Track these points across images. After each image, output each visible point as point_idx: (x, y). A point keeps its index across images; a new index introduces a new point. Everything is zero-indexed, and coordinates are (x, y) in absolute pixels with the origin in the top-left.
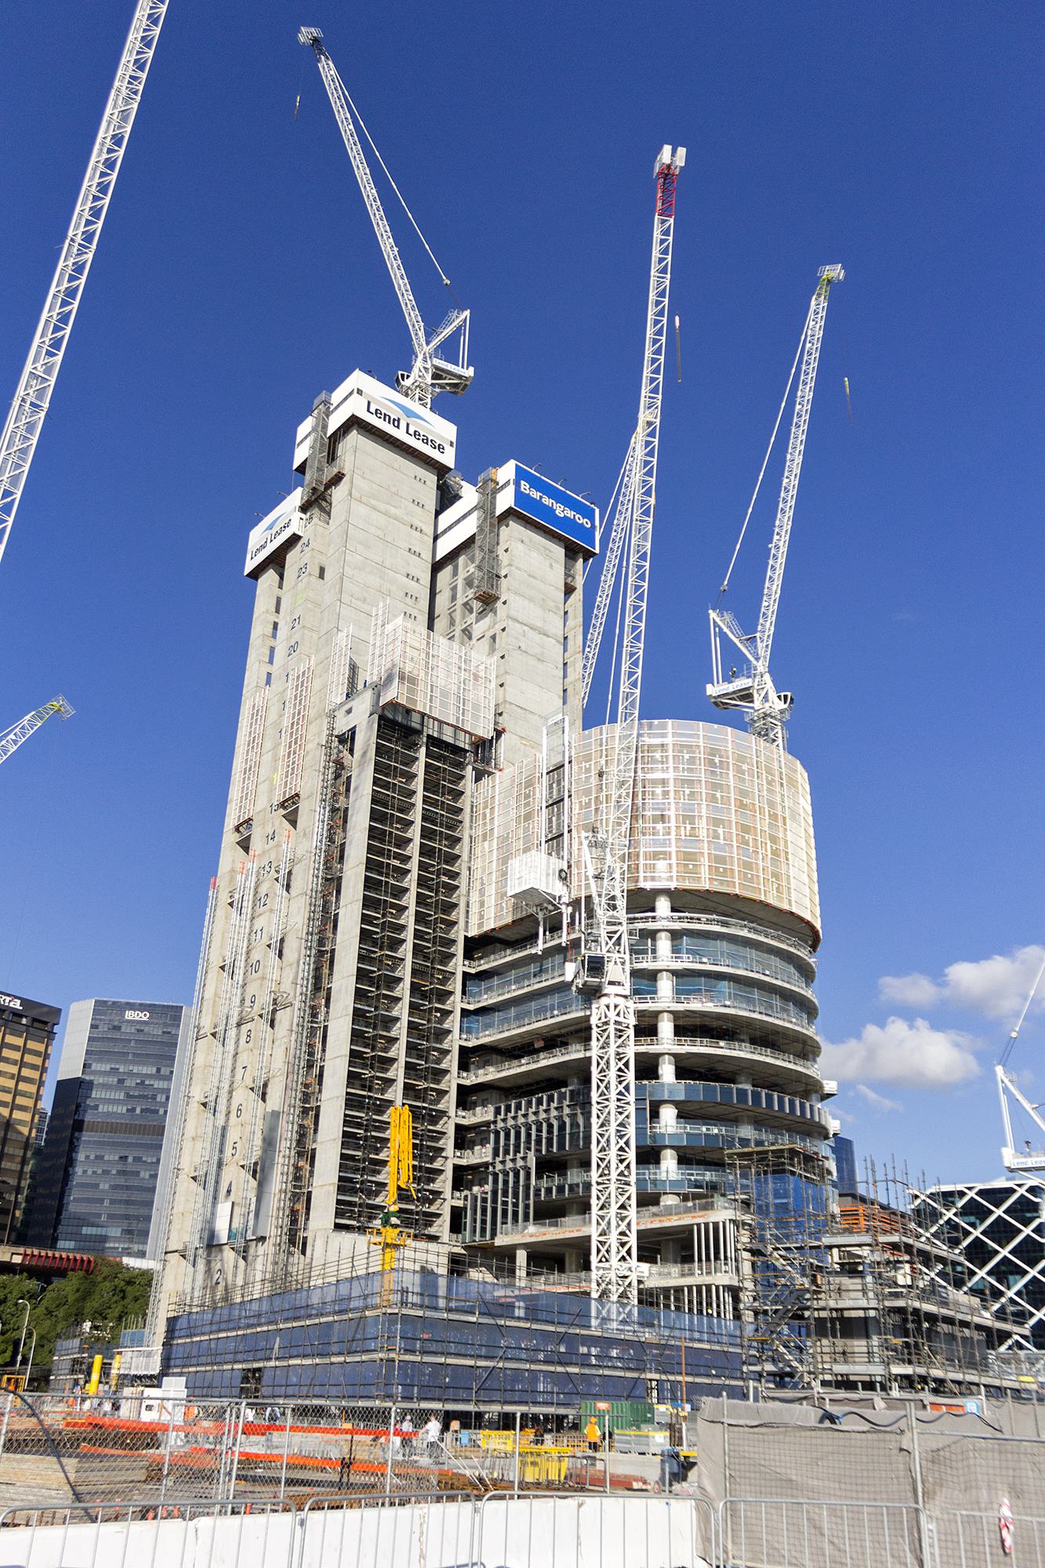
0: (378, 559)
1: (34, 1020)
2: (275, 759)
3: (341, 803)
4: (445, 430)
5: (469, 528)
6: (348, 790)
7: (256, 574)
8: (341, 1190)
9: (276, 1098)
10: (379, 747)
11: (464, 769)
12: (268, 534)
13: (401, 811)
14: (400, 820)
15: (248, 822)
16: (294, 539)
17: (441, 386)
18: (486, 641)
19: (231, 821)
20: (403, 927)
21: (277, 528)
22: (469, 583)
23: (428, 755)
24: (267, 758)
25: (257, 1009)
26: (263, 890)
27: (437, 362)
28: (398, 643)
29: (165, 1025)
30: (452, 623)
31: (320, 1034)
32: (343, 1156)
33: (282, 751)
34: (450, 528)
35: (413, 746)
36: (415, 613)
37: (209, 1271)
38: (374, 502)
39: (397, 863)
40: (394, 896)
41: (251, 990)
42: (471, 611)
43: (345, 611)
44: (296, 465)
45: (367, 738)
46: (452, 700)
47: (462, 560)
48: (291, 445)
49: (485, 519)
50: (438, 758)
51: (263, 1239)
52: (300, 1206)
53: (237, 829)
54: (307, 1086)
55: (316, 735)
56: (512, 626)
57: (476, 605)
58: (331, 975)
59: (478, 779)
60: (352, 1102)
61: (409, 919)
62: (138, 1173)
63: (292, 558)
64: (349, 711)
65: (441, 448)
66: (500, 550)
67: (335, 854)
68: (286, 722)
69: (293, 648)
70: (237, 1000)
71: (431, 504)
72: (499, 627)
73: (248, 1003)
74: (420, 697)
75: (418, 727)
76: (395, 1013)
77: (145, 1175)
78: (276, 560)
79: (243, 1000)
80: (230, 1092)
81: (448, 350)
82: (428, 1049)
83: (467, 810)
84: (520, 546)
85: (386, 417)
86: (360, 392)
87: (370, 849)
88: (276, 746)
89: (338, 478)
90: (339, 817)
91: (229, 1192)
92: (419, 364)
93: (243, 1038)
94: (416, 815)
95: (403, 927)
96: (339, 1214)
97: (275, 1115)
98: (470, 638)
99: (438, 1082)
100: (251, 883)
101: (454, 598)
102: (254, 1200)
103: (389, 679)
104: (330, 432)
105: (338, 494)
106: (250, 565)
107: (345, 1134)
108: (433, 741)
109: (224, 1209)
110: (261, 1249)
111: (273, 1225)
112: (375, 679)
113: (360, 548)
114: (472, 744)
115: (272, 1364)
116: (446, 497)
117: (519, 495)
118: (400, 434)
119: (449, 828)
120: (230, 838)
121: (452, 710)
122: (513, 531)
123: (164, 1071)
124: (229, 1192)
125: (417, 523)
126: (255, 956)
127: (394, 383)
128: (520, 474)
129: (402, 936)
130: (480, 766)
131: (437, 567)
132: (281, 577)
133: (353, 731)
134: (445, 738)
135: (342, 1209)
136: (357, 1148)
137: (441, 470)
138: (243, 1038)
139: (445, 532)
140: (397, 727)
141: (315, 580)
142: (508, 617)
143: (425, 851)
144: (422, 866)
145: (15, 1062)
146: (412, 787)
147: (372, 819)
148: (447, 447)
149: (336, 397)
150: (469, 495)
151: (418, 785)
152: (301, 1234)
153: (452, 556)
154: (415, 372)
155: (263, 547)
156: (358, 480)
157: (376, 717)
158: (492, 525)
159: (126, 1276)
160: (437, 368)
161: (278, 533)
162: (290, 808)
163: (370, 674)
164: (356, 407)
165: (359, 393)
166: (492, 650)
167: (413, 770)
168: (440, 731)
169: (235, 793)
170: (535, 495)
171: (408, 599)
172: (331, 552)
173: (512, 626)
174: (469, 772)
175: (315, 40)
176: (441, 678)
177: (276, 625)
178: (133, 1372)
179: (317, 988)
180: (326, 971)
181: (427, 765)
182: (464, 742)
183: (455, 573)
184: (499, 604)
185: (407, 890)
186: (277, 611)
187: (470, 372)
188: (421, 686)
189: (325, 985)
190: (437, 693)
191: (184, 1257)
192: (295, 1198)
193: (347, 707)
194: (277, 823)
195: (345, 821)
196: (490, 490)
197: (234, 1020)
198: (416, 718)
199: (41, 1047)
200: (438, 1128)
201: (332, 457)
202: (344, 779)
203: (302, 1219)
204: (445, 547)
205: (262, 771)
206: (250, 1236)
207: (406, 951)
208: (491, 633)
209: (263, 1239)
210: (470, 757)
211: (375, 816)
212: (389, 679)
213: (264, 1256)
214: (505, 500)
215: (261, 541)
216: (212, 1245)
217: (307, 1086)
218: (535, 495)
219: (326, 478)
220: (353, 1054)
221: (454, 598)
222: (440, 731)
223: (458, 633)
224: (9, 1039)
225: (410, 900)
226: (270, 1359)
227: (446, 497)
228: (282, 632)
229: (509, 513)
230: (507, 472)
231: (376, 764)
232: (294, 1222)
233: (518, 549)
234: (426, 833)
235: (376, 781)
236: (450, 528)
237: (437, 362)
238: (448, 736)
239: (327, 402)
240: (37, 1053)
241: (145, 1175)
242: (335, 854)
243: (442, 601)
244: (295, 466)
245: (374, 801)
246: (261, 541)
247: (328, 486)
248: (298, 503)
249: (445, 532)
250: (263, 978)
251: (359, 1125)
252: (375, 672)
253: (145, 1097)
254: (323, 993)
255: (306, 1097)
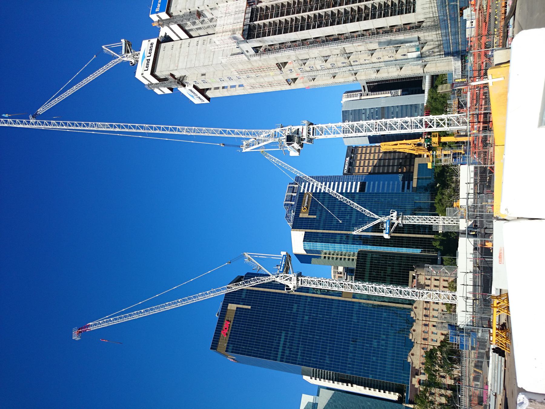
0: (195, 56)
1: (352, 153)
2: (266, 76)
3: (278, 46)
4: (146, 44)
5: (175, 27)
6: (272, 45)
7: (208, 99)
8: (402, 13)
9: (375, 46)
10: (257, 37)
11: (258, 8)
12: (195, 97)
13: (276, 25)
14: (280, 25)
15: (287, 81)
16: (195, 87)
17: (131, 50)
18: (213, 12)
19: (288, 87)
20: (315, 15)
21: (192, 94)
22: (194, 23)
23: (256, 20)
24: (266, 79)
25: (347, 61)
26: (308, 69)
27: (123, 52)
28: (223, 39)
29: (349, 115)
30: (209, 27)
31: (353, 34)
32: (391, 15)
33: (263, 74)
34: (177, 35)
35: (254, 26)
36: (209, 40)
37: (429, 56)
38: (177, 62)
39: (294, 23)
40: (305, 21)
41: (340, 65)
42: (204, 20)
43: (214, 62)
44: (170, 92)
45: (255, 42)
46: (236, 16)
47: (187, 28)
48: (165, 95)
49: (172, 22)
50: (256, 17)
51: (419, 38)
52: (408, 27)
53: (290, 84)
54: (370, 35)
55: (258, 61)
56: (206, 4)
57: (202, 19)
58: (332, 35)
59: (261, 2)
60: (373, 17)
61: (311, 14)
62: (397, 112)
63: (201, 87)
64: (247, 51)
65: (152, 44)
66: (181, 14)
67: (295, 45)
68: (253, 75)
69: (230, 79)
70: (344, 69)
71: (171, 43)
72: (208, 8)
73: (345, 65)
74: (238, 27)
75: (248, 26)
76: (343, 11)
77: (397, 110)
78: (202, 92)
79: (344, 67)
80: (373, 63)
81: (118, 50)
82: (351, 15)
83: (272, 3)
84: (178, 7)
85: (148, 64)
86: (142, 74)
87: (291, 31)
88: (262, 77)
89: (172, 75)
90: (282, 46)
91: (404, 55)
92: (125, 59)
93: (356, 63)
94: (277, 19)
95: (315, 15)
96: (410, 12)
97: (380, 43)
98: (213, 19)
99: (362, 9)
100: (307, 74)
101: (200, 28)
102: (406, 44)
103: (235, 38)
104: (158, 82)
105: (177, 75)
106: (206, 101)
107: (384, 16)
108: (251, 20)
109: (410, 55)
110: (422, 39)
111: (414, 35)
112: (235, 44)
113: (193, 62)
114: (249, 7)
115: (458, 4)
116: (168, 39)
117: (161, 11)
118: (152, 58)
119: (279, 8)
120: (293, 86)
121: (240, 15)
122: (174, 10)
123: (363, 111)
124: (404, 55)
125: (179, 46)
126: (330, 66)
127: (135, 66)
128: (154, 12)
129: (317, 15)
130: (256, 2)
131: (191, 37)
132: (207, 89)
133: (253, 48)
134: (249, 16)
135: (408, 11)
136: (388, 12)
137: (159, 43)
138: (356, 63)
139: (179, 37)
140: (250, 33)
141: (207, 76)
142: (203, 5)
143: (288, 14)
144: (293, 13)
145: (366, 155)
146: (268, 24)
147: (281, 33)
148: (151, 42)
149: (146, 82)
150: (164, 31)
151: (267, 21)
152: (417, 24)
153: (186, 32)
154: (129, 59)
155: (199, 98)
156: (171, 68)
157: (248, 41)
158: (173, 19)
159: (430, 99)
160: (125, 52)
161: (194, 93)
162: (281, 66)
163: (233, 46)
164: (148, 74)
165: (142, 74)
166: (215, 8)
167: (262, 25)
168: (248, 18)
169: (278, 88)
170: (159, 5)
171: (205, 43)
172: (196, 72)
173: (206, 4)
174: (259, 5)
175: (33, 117)
176: (231, 20)
177: (223, 88)
178: (460, 73)
179: (338, 39)
180: (332, 37)
181: (259, 20)
182: (250, 10)
183: (191, 30)
184: (199, 10)
185: (302, 17)
186: (232, 55)
187: (123, 41)
188: (235, 27)
189: (337, 37)
190: (236, 21)
191: (426, 65)
192: (405, 29)
193: (246, 53)
194: (286, 70)
195: (283, 43)
196: (162, 23)
197: (350, 68)
198: (245, 27)
199: (360, 149)
200: (377, 6)
201: (165, 79)
202: (269, 47)
203: (411, 25)
204: (184, 35)
205: (270, 80)
206: (417, 43)
207: (322, 12)
208: (210, 10)
209: (419, 38)
210: (254, 6)
211: (280, 33)
212: (235, 38)
213: (423, 35)
214: (164, 16)
215: (197, 99)
216: (421, 57)
217: (370, 35)
218: (159, 5)
219: (173, 80)
220: (358, 20)
221: (200, 28)
222: (248, 18)
223: (212, 24)
224: (357, 171)
225: (305, 15)
226: (457, 5)
227: (168, 39)
228: (225, 84)
229: (168, 13)
230: (154, 17)
231: (263, 36)
232: (413, 28)
233: (179, 7)
234: (282, 15)
235: (269, 35)
236: (177, 35)
237: (123, 52)
238: (249, 15)
239: (148, 85)
240: (362, 150)
241: (397, 110)
242: (295, 45)
243: (202, 32)
244: (171, 92)
245: (275, 34)
246: (197, 99)
247: (176, 79)
248: (183, 88)
249: (179, 37)
250: (336, 61)
251: (381, 13)
252: (233, 45)
253: (372, 116)
254: (340, 36)
255: (373, 34)
